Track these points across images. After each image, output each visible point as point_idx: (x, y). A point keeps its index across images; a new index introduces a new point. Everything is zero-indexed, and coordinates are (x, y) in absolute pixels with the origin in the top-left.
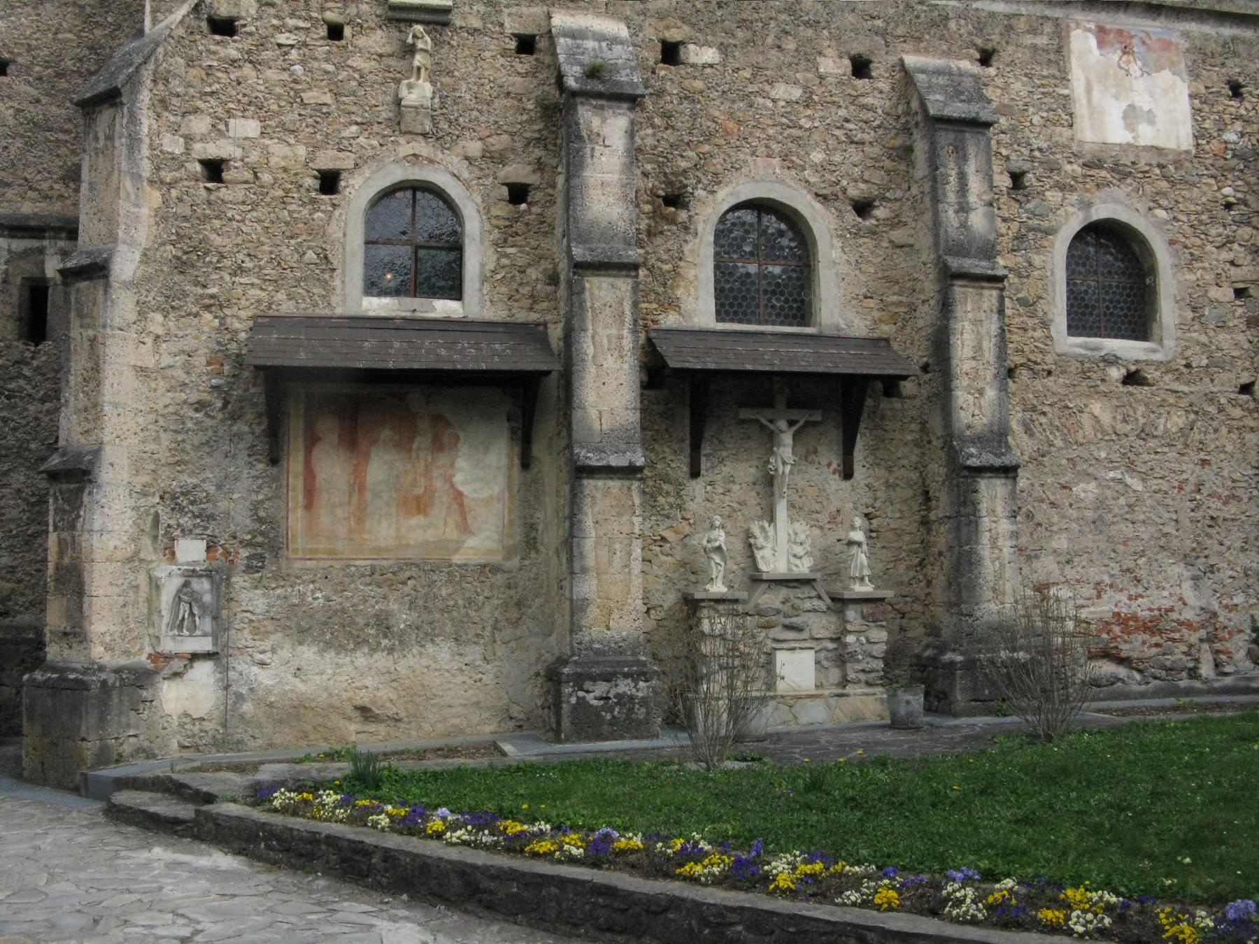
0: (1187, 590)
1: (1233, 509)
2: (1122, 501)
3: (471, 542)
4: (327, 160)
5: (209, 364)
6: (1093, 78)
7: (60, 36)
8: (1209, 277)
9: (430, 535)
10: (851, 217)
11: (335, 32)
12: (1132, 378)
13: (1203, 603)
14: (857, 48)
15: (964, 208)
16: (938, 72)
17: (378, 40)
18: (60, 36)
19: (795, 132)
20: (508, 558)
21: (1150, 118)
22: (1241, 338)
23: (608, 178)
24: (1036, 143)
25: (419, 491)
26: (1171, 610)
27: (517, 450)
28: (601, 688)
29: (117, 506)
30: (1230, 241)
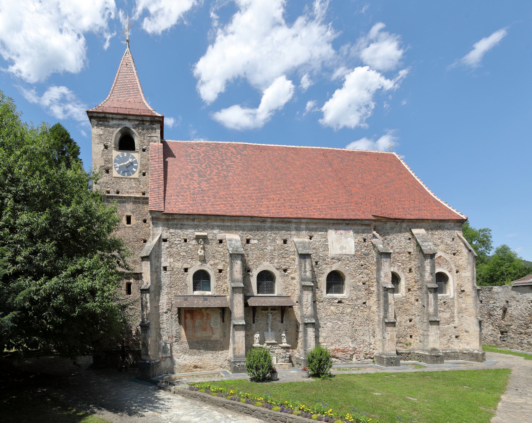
0: (350, 344)
1: (361, 328)
2: (337, 326)
3: (214, 336)
4: (185, 266)
5: (167, 305)
6: (334, 240)
8: (357, 280)
9: (207, 335)
10: (283, 272)
11: (185, 241)
12: (340, 302)
13: (354, 346)
14: (284, 238)
15: (305, 272)
16: (301, 243)
17: (194, 242)
19: (272, 256)
20: (220, 339)
21: (345, 248)
22: (364, 293)
23: (237, 270)
24: (321, 255)
25: (204, 327)
26: (347, 348)
27: (222, 319)
28: (238, 364)
29: (153, 332)
30: (362, 273)
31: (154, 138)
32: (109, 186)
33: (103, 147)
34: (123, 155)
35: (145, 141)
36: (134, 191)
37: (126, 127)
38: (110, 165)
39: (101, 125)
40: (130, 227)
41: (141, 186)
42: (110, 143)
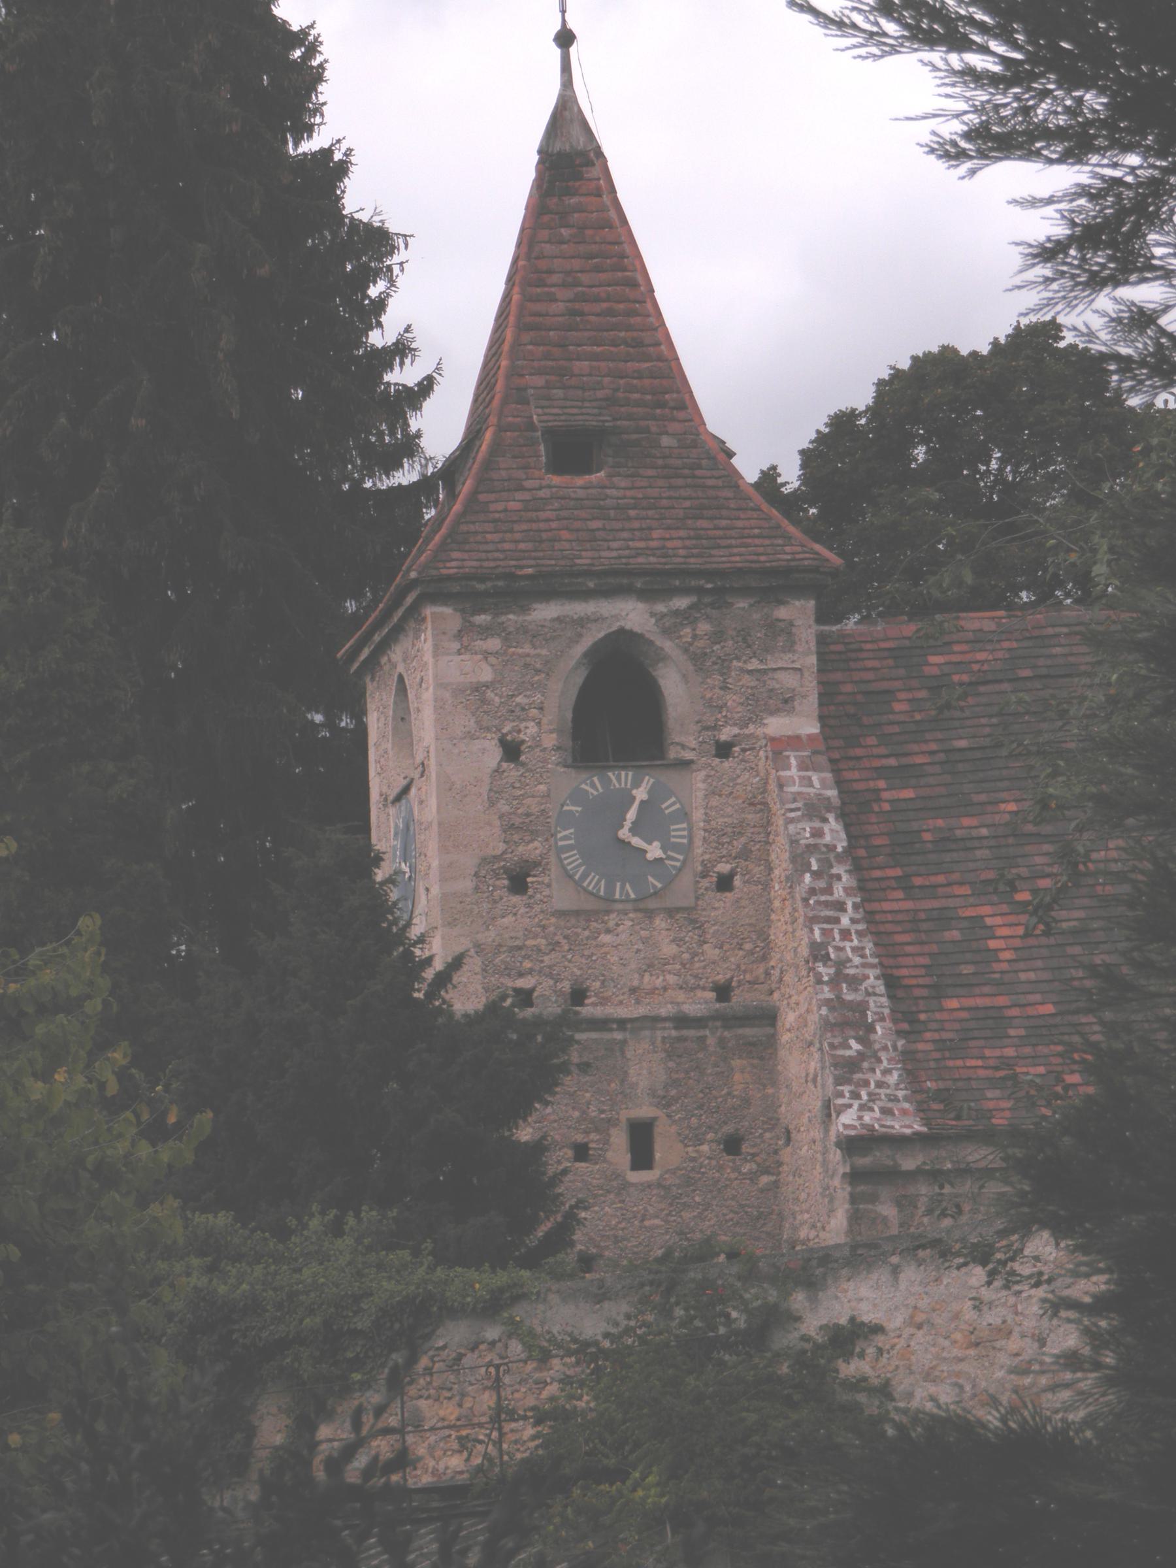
7: (647, 1223)
18: (647, 1223)
31: (780, 675)
32: (527, 964)
33: (493, 755)
34: (606, 782)
35: (731, 700)
36: (672, 979)
37: (622, 631)
38: (533, 849)
39: (485, 632)
40: (649, 1186)
41: (711, 952)
42: (532, 729)
